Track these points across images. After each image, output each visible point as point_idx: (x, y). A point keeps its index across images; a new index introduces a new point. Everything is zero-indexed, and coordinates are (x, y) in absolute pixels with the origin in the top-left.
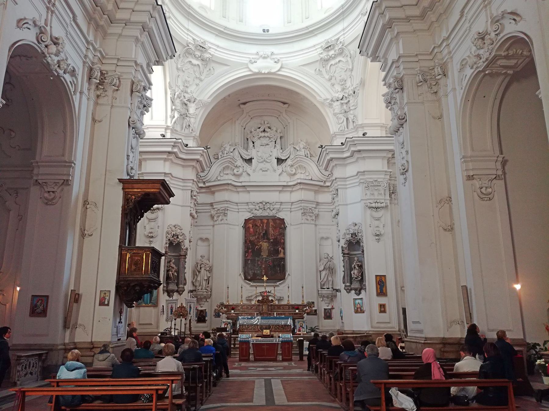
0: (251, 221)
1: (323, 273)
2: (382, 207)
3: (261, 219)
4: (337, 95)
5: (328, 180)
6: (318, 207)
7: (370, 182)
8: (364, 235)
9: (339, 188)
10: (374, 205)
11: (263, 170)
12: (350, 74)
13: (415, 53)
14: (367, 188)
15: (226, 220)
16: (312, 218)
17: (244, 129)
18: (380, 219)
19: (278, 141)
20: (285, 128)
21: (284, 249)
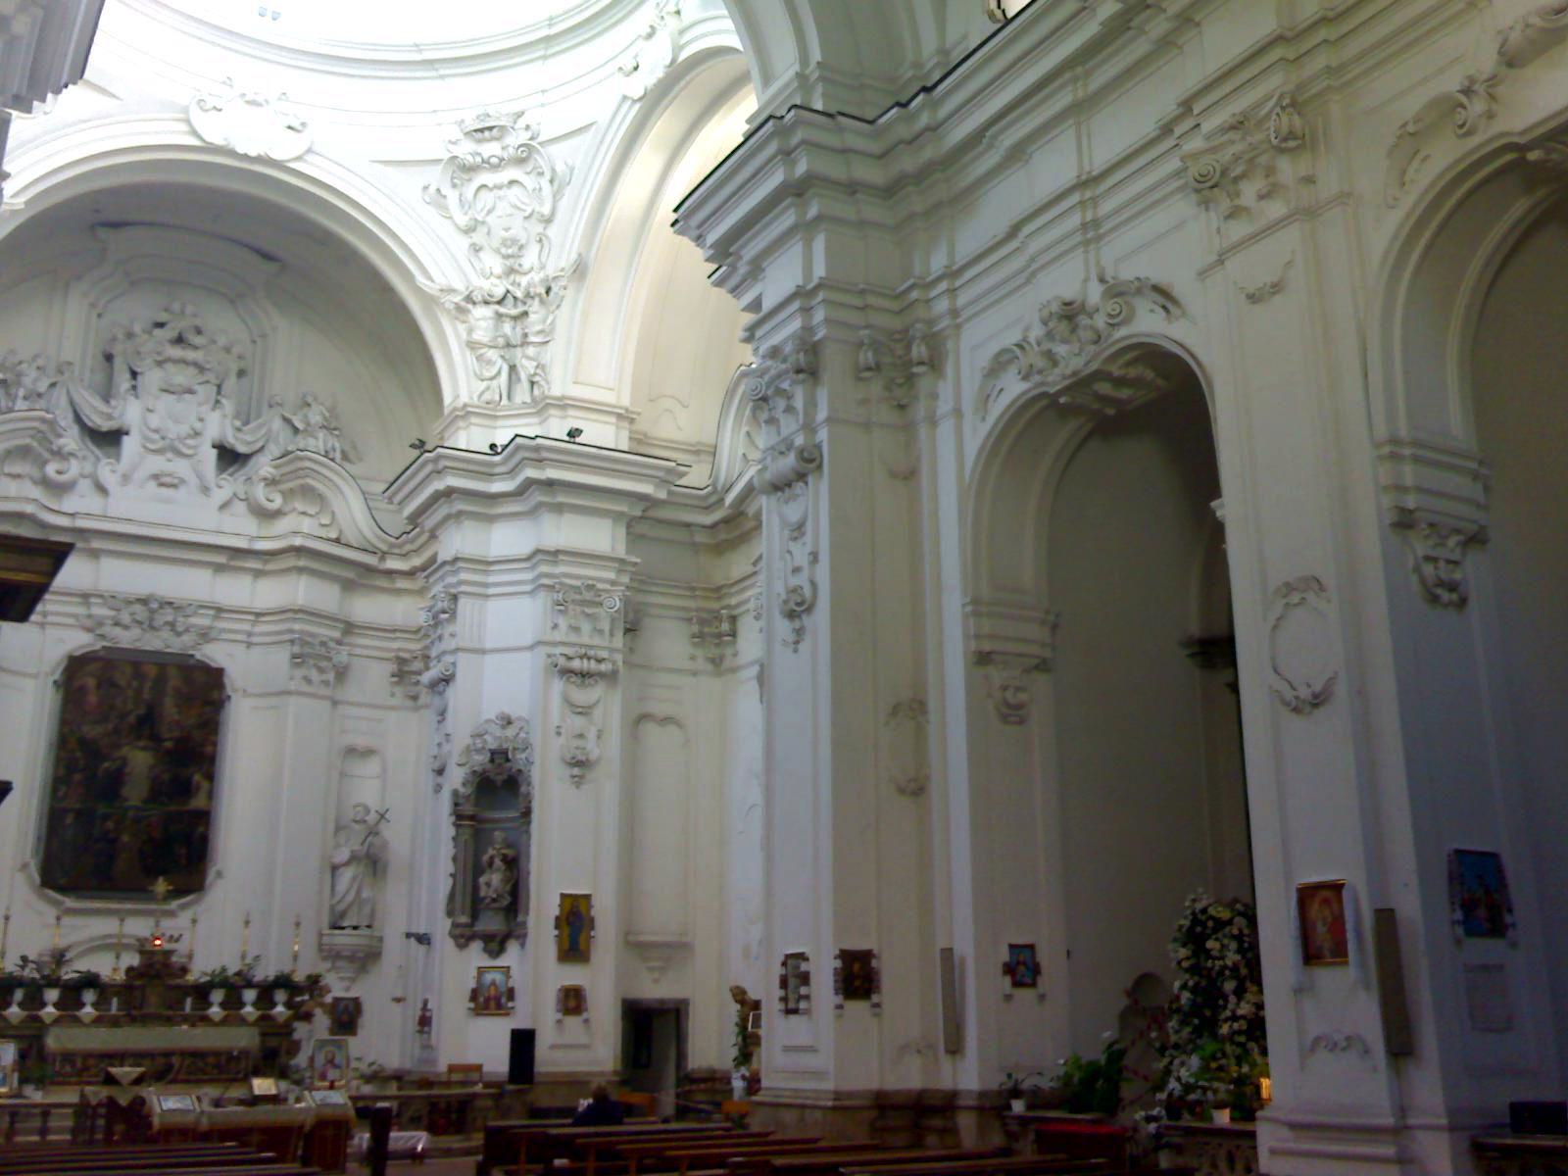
0: (93, 667)
1: (347, 875)
2: (601, 675)
3: (136, 661)
5: (396, 551)
6: (347, 640)
8: (537, 758)
9: (462, 593)
10: (576, 664)
12: (541, 230)
14: (562, 608)
16: (324, 677)
18: (589, 711)
19: (231, 382)
21: (210, 777)
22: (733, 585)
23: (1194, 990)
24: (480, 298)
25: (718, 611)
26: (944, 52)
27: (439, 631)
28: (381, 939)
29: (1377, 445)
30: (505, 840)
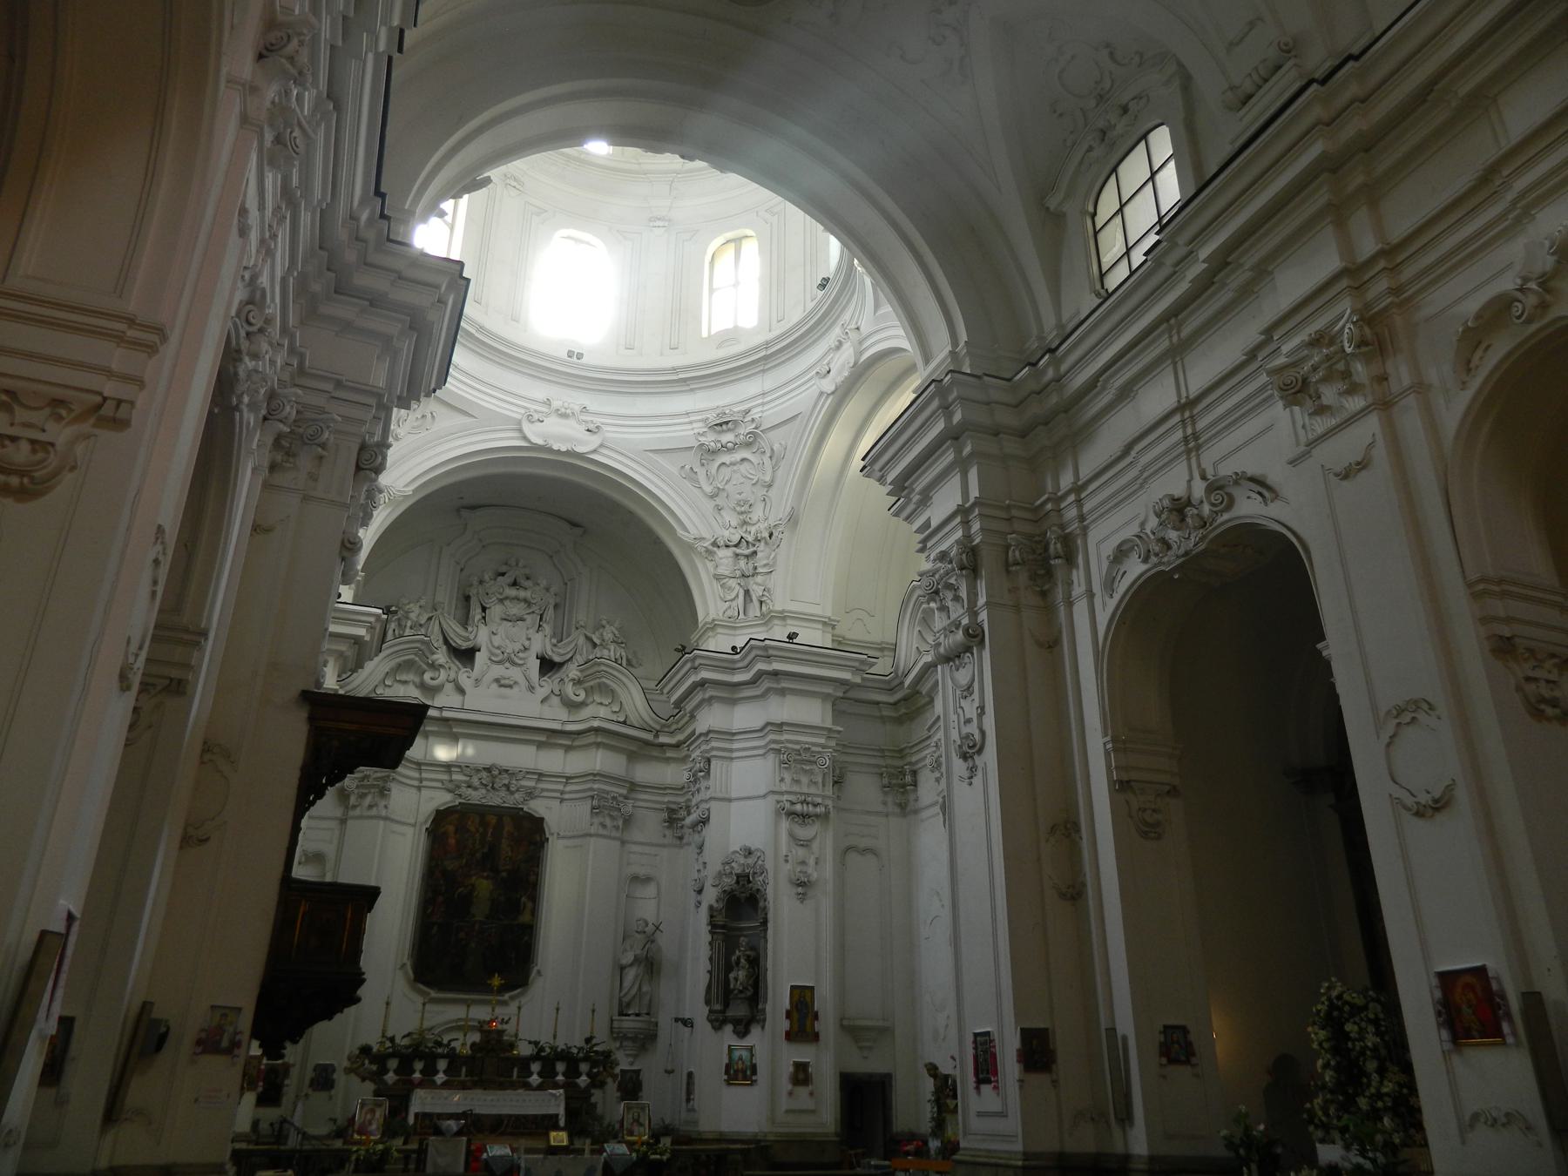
1: (631, 974)
2: (817, 816)
3: (482, 811)
4: (726, 533)
5: (666, 730)
6: (634, 795)
7: (793, 750)
10: (798, 807)
11: (503, 682)
12: (765, 493)
13: (1007, 502)
15: (386, 807)
17: (462, 570)
19: (550, 614)
20: (566, 584)
22: (913, 746)
23: (1337, 1069)
24: (722, 543)
25: (902, 767)
26: (1060, 326)
27: (697, 786)
28: (656, 1024)
29: (1470, 585)
30: (747, 944)
